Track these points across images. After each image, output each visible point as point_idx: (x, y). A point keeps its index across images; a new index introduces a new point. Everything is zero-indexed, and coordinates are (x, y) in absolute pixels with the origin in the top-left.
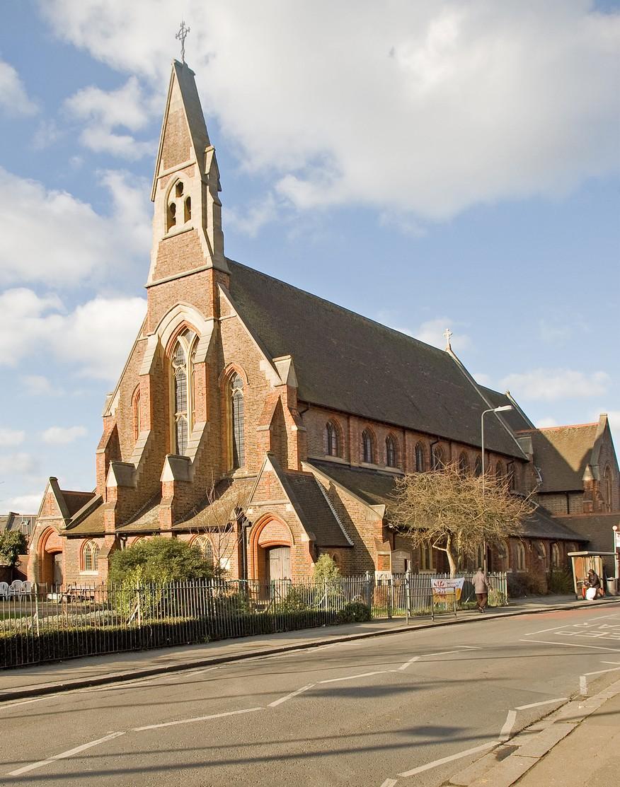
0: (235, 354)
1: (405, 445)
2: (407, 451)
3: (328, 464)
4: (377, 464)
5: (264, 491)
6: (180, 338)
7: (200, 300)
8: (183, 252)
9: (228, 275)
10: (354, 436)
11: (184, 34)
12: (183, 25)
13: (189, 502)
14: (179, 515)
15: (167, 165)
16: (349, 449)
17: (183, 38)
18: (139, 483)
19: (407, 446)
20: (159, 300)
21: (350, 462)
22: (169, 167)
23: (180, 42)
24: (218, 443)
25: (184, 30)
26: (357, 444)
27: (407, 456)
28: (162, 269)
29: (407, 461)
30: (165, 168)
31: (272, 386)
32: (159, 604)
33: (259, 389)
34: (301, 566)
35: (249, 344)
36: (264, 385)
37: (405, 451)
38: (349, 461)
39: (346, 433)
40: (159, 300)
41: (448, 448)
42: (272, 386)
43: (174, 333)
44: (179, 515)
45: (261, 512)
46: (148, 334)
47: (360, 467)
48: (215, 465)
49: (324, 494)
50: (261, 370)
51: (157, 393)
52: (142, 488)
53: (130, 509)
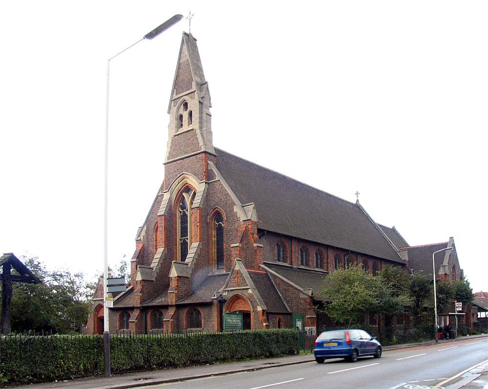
1: (328, 256)
5: (234, 282)
6: (184, 194)
7: (197, 171)
14: (181, 297)
15: (178, 92)
16: (292, 258)
22: (179, 93)
45: (232, 294)
46: (164, 191)
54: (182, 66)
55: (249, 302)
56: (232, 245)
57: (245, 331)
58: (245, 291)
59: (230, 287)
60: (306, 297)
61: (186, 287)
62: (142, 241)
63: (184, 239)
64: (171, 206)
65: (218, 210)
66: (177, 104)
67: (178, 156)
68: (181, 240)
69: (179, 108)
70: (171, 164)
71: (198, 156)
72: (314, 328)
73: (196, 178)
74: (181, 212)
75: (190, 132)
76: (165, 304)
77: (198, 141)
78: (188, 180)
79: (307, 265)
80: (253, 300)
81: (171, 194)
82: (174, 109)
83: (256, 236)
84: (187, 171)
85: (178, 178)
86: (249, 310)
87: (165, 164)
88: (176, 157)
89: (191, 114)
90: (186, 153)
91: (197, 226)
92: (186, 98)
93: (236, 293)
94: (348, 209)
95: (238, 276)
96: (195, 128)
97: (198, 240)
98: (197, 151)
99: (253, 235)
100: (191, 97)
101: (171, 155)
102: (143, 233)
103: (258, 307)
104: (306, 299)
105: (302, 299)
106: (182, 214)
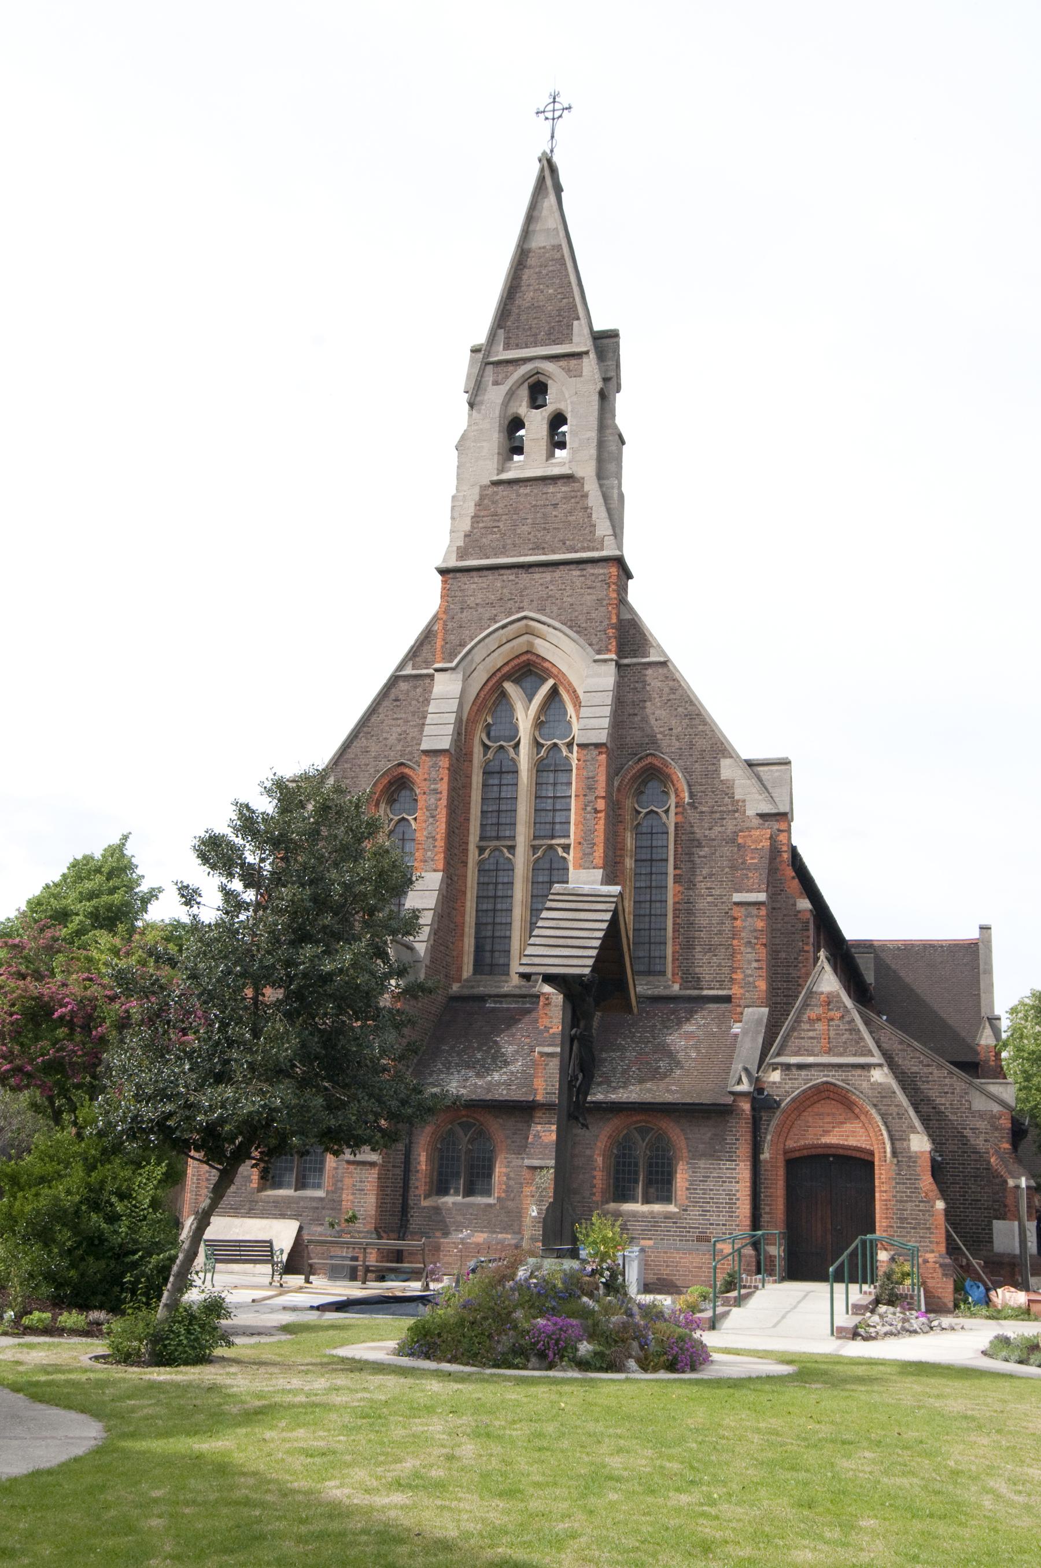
5: (811, 1034)
6: (509, 687)
7: (582, 618)
11: (557, 113)
15: (512, 341)
22: (518, 346)
25: (557, 106)
30: (507, 347)
31: (750, 812)
33: (718, 815)
35: (697, 722)
36: (730, 808)
42: (750, 812)
43: (499, 675)
45: (801, 1083)
46: (437, 665)
49: (983, 1081)
54: (531, 261)
55: (878, 1118)
56: (737, 897)
57: (299, 1193)
58: (859, 1072)
59: (797, 1054)
60: (996, 1108)
63: (496, 849)
64: (461, 720)
66: (507, 377)
67: (503, 551)
69: (511, 394)
73: (582, 641)
76: (516, 1094)
77: (590, 516)
78: (538, 642)
80: (894, 1110)
81: (465, 679)
82: (494, 395)
84: (541, 610)
85: (503, 627)
86: (865, 1144)
87: (443, 572)
88: (496, 555)
89: (558, 420)
90: (538, 548)
91: (596, 811)
93: (820, 1078)
95: (831, 1014)
96: (579, 473)
97: (441, 866)
100: (568, 371)
101: (470, 544)
103: (912, 1136)
104: (993, 1117)
105: (981, 1115)
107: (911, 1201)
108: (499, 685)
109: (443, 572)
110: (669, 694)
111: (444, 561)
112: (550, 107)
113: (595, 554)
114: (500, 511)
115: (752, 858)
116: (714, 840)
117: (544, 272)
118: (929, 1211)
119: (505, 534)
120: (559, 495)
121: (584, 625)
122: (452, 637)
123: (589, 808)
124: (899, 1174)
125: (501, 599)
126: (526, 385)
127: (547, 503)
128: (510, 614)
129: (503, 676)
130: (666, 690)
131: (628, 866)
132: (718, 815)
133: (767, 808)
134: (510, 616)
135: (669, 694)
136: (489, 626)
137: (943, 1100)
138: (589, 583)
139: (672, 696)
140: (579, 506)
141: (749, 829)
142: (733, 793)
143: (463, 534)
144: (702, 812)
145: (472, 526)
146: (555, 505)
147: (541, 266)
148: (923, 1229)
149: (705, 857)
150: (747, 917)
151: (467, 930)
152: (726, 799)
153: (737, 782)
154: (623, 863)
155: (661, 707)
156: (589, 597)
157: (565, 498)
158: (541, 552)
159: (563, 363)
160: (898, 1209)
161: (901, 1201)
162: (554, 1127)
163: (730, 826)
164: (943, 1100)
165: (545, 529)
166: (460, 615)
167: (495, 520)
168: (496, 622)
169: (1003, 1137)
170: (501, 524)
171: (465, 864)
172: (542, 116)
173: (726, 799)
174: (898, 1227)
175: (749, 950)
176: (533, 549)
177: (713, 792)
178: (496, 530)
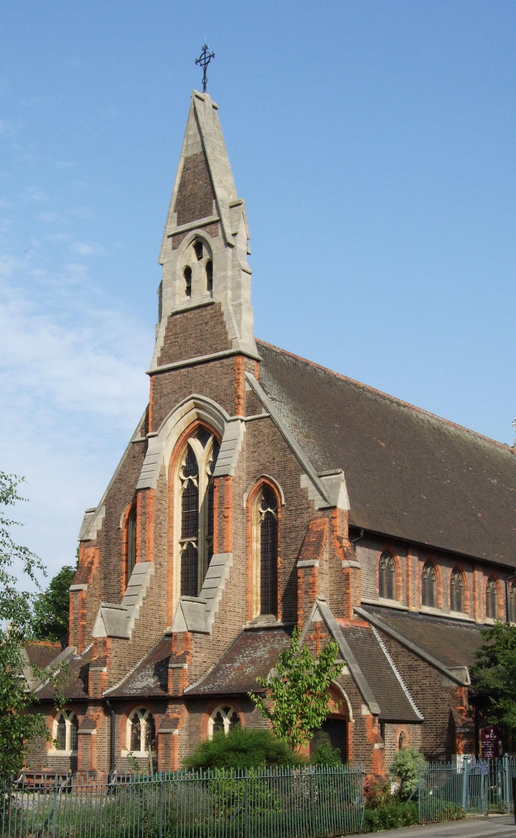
0: (268, 464)
1: (474, 582)
2: (477, 590)
3: (383, 610)
4: (441, 608)
7: (222, 394)
8: (201, 332)
9: (258, 361)
10: (414, 572)
11: (207, 60)
12: (205, 49)
13: (205, 660)
14: (194, 677)
16: (408, 589)
17: (206, 64)
18: (134, 632)
19: (477, 584)
20: (165, 391)
21: (408, 606)
22: (184, 222)
23: (201, 69)
24: (241, 580)
25: (207, 55)
26: (416, 582)
27: (477, 595)
28: (171, 352)
29: (477, 603)
31: (316, 508)
32: (230, 800)
33: (300, 511)
34: (361, 747)
36: (306, 506)
37: (474, 590)
38: (408, 605)
39: (405, 568)
40: (165, 391)
41: (504, 584)
43: (184, 435)
44: (194, 677)
47: (420, 613)
48: (237, 610)
50: (301, 487)
51: (159, 513)
52: (137, 639)
53: (122, 668)
61: (203, 655)
62: (94, 543)
65: (267, 482)
68: (182, 544)
70: (167, 374)
71: (225, 361)
72: (60, 645)
74: (261, 513)
75: (209, 308)
77: (225, 328)
79: (432, 603)
83: (346, 543)
87: (151, 374)
88: (177, 360)
90: (199, 352)
92: (201, 232)
94: (333, 379)
98: (222, 350)
99: (341, 542)
102: (98, 524)
105: (447, 689)
106: (185, 486)
107: (362, 745)
108: (185, 441)
109: (151, 374)
110: (273, 436)
111: (151, 368)
112: (203, 57)
113: (227, 352)
114: (178, 331)
115: (313, 538)
116: (298, 527)
117: (197, 171)
118: (370, 750)
119: (181, 346)
120: (208, 316)
121: (223, 398)
122: (156, 415)
123: (221, 516)
124: (356, 729)
125: (180, 388)
126: (191, 246)
127: (202, 322)
128: (185, 396)
129: (186, 435)
130: (272, 434)
131: (255, 548)
132: (300, 511)
133: (324, 505)
134: (185, 397)
135: (273, 436)
136: (175, 406)
137: (425, 682)
138: (225, 371)
139: (275, 438)
140: (219, 322)
141: (316, 518)
142: (307, 497)
143: (160, 349)
144: (291, 510)
145: (165, 344)
146: (206, 323)
147: (195, 167)
148: (368, 760)
149: (293, 538)
150: (305, 575)
151: (174, 594)
152: (304, 500)
153: (309, 489)
154: (251, 546)
155: (269, 445)
156: (225, 380)
157: (211, 317)
158: (200, 354)
159: (208, 228)
160: (355, 750)
161: (357, 745)
162: (337, 712)
163: (306, 517)
164: (425, 682)
165: (201, 339)
166: (160, 401)
167: (175, 338)
168: (178, 403)
169: (458, 703)
170: (179, 340)
171: (171, 554)
172: (199, 63)
173: (304, 500)
174: (355, 760)
175: (306, 596)
176: (195, 353)
177: (297, 497)
178: (176, 343)
